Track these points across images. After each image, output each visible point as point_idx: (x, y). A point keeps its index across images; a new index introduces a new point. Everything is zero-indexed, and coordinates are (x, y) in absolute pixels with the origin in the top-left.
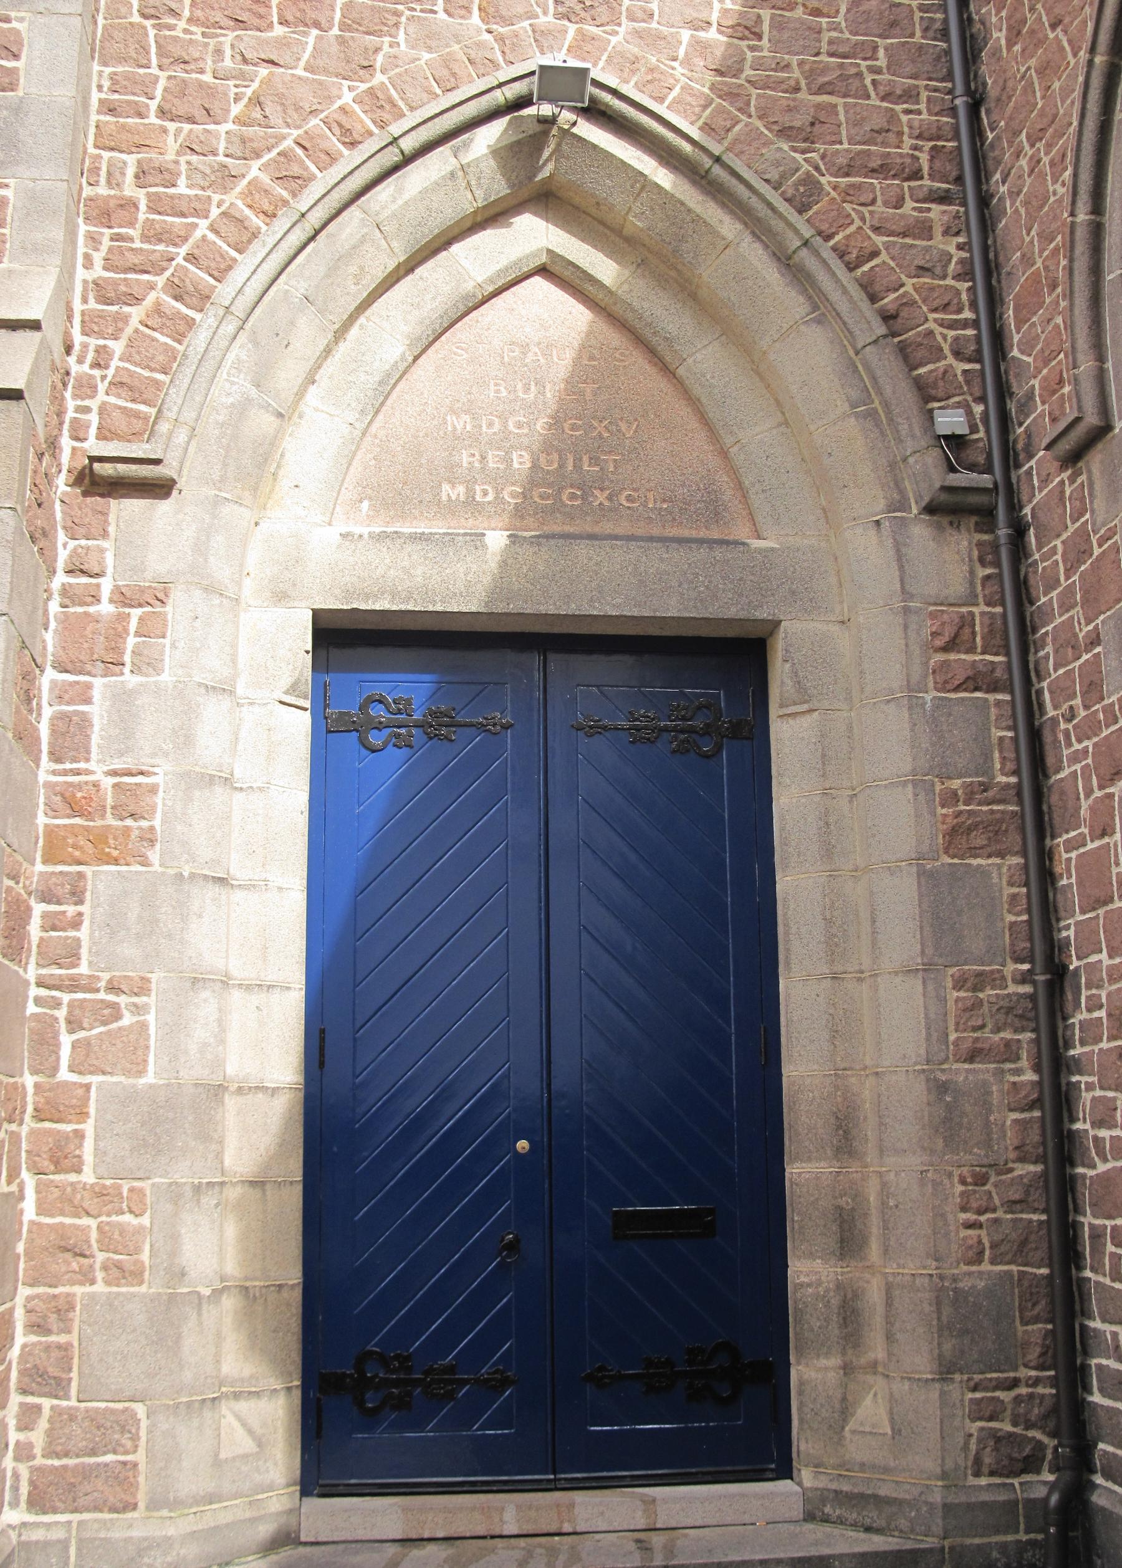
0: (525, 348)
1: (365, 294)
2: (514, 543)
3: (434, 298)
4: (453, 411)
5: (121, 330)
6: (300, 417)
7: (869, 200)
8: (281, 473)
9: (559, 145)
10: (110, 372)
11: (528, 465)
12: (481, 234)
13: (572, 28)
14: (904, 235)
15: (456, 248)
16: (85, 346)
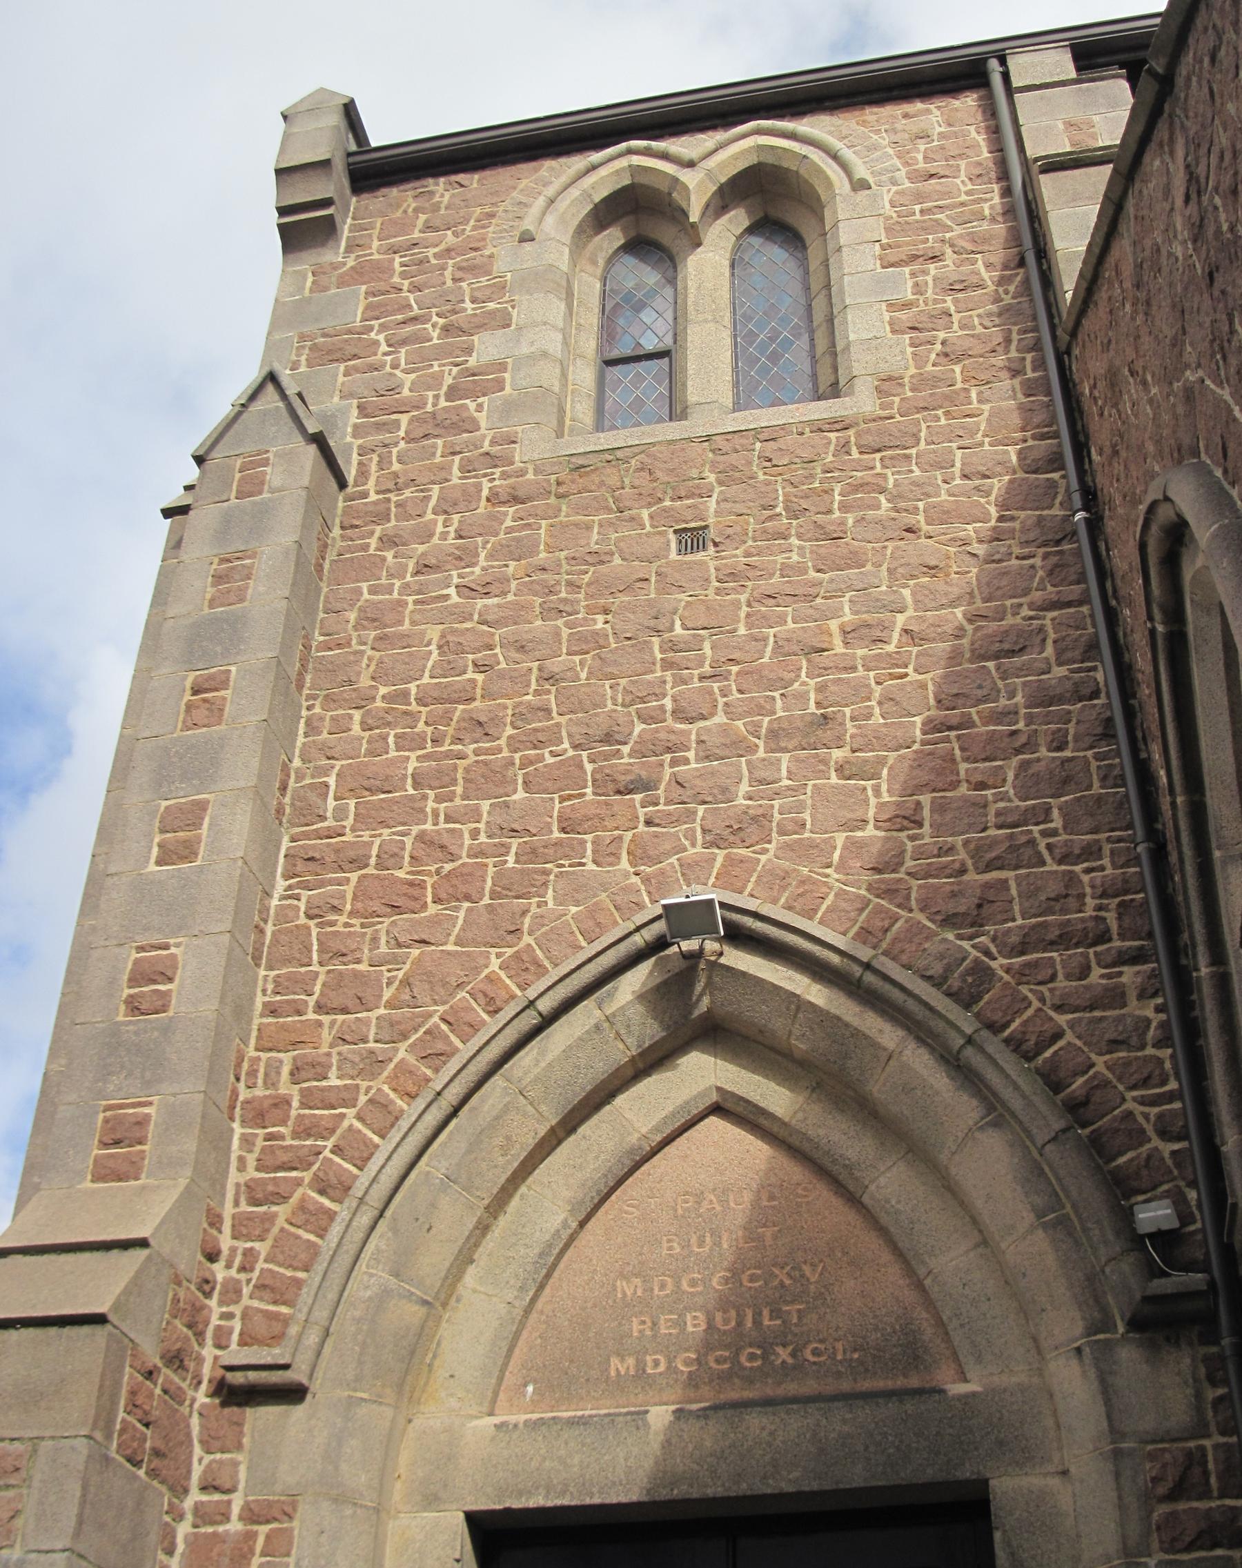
0: (699, 1197)
1: (516, 1164)
2: (678, 1419)
3: (597, 1157)
4: (622, 1276)
5: (268, 1230)
6: (458, 1301)
7: (1048, 977)
8: (437, 1363)
9: (710, 978)
10: (256, 1273)
11: (703, 1326)
12: (645, 1081)
13: (720, 855)
14: (1092, 1008)
15: (620, 1100)
16: (233, 1250)
